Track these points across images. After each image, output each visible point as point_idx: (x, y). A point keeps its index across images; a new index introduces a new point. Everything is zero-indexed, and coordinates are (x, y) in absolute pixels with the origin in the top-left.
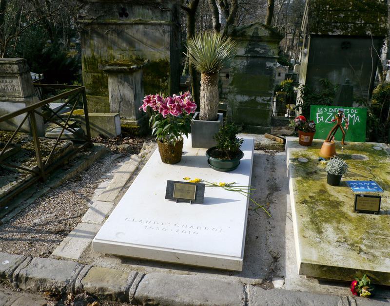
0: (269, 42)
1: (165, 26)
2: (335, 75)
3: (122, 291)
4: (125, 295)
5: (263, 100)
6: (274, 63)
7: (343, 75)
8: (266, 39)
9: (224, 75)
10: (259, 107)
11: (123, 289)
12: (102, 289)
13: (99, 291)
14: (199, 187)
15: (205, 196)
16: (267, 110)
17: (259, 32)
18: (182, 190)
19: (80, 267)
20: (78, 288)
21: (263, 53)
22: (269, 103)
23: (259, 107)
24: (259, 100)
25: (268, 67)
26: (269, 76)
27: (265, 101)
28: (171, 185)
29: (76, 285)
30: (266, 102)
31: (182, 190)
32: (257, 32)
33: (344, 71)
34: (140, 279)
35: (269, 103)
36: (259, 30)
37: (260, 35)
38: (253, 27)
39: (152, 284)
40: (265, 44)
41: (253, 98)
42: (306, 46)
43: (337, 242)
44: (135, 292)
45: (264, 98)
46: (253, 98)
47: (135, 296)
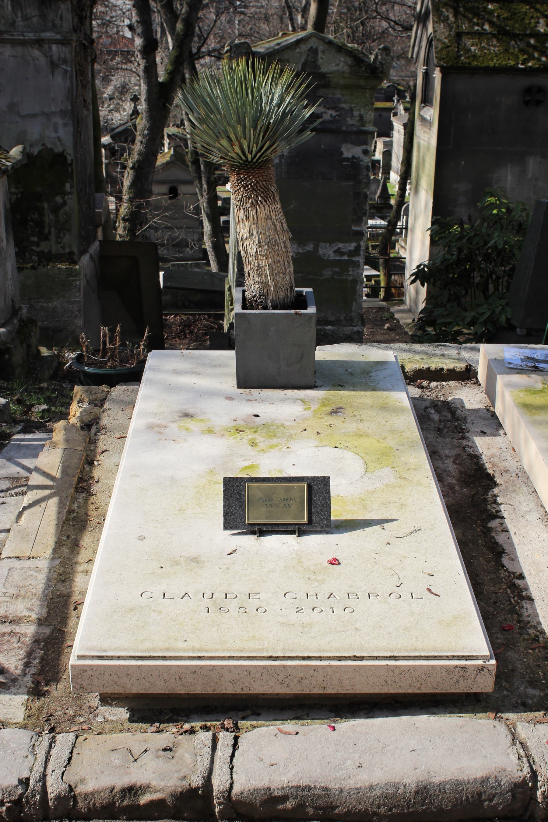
0: (347, 87)
1: (54, 47)
2: (509, 178)
3: (194, 785)
4: (202, 797)
5: (338, 252)
6: (364, 147)
7: (530, 175)
8: (342, 82)
9: (164, 189)
10: (327, 273)
11: (196, 781)
12: (131, 791)
13: (123, 799)
14: (317, 489)
15: (333, 518)
16: (350, 278)
17: (320, 61)
18: (268, 500)
19: (46, 743)
20: (58, 798)
21: (333, 120)
22: (354, 259)
23: (327, 273)
24: (328, 251)
25: (347, 159)
26: (351, 183)
27: (343, 254)
28: (234, 489)
29: (49, 790)
30: (346, 258)
31: (268, 500)
32: (315, 62)
33: (533, 164)
34: (231, 748)
35: (354, 259)
36: (320, 55)
37: (324, 70)
38: (304, 47)
39: (270, 758)
40: (338, 94)
41: (310, 247)
42: (427, 101)
43: (145, 764)
44: (231, 785)
45: (341, 245)
46: (310, 247)
47: (234, 791)
